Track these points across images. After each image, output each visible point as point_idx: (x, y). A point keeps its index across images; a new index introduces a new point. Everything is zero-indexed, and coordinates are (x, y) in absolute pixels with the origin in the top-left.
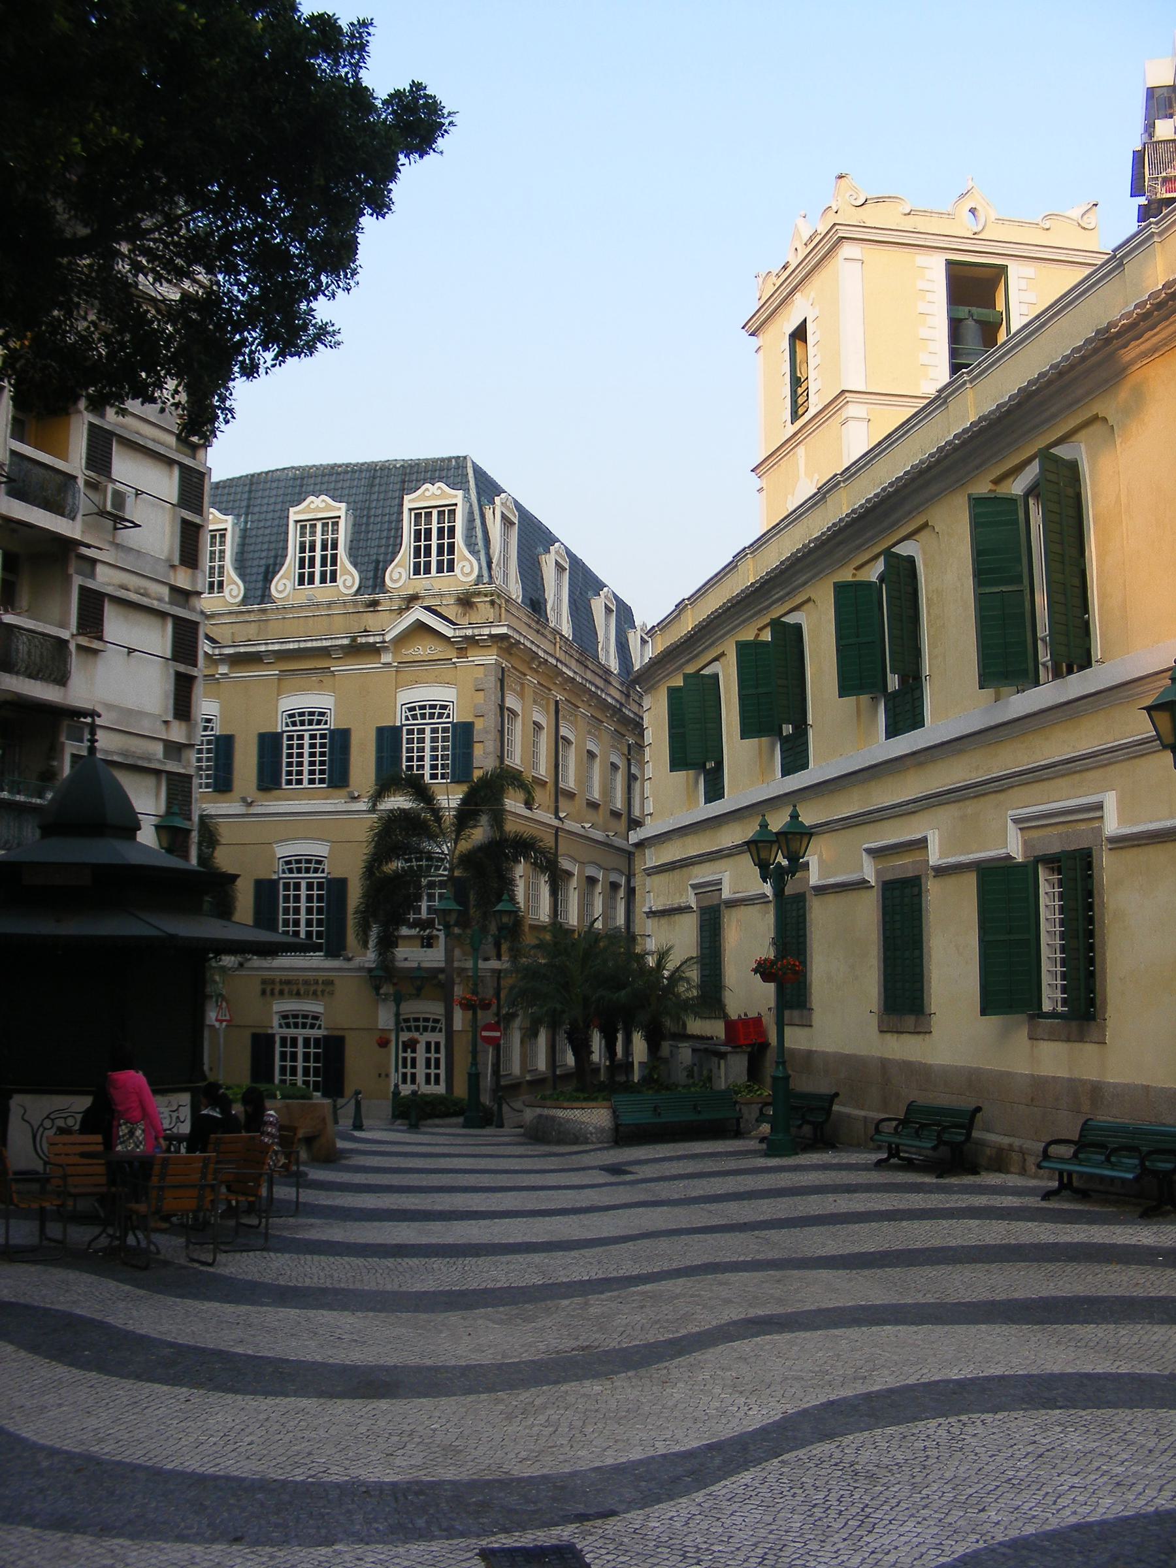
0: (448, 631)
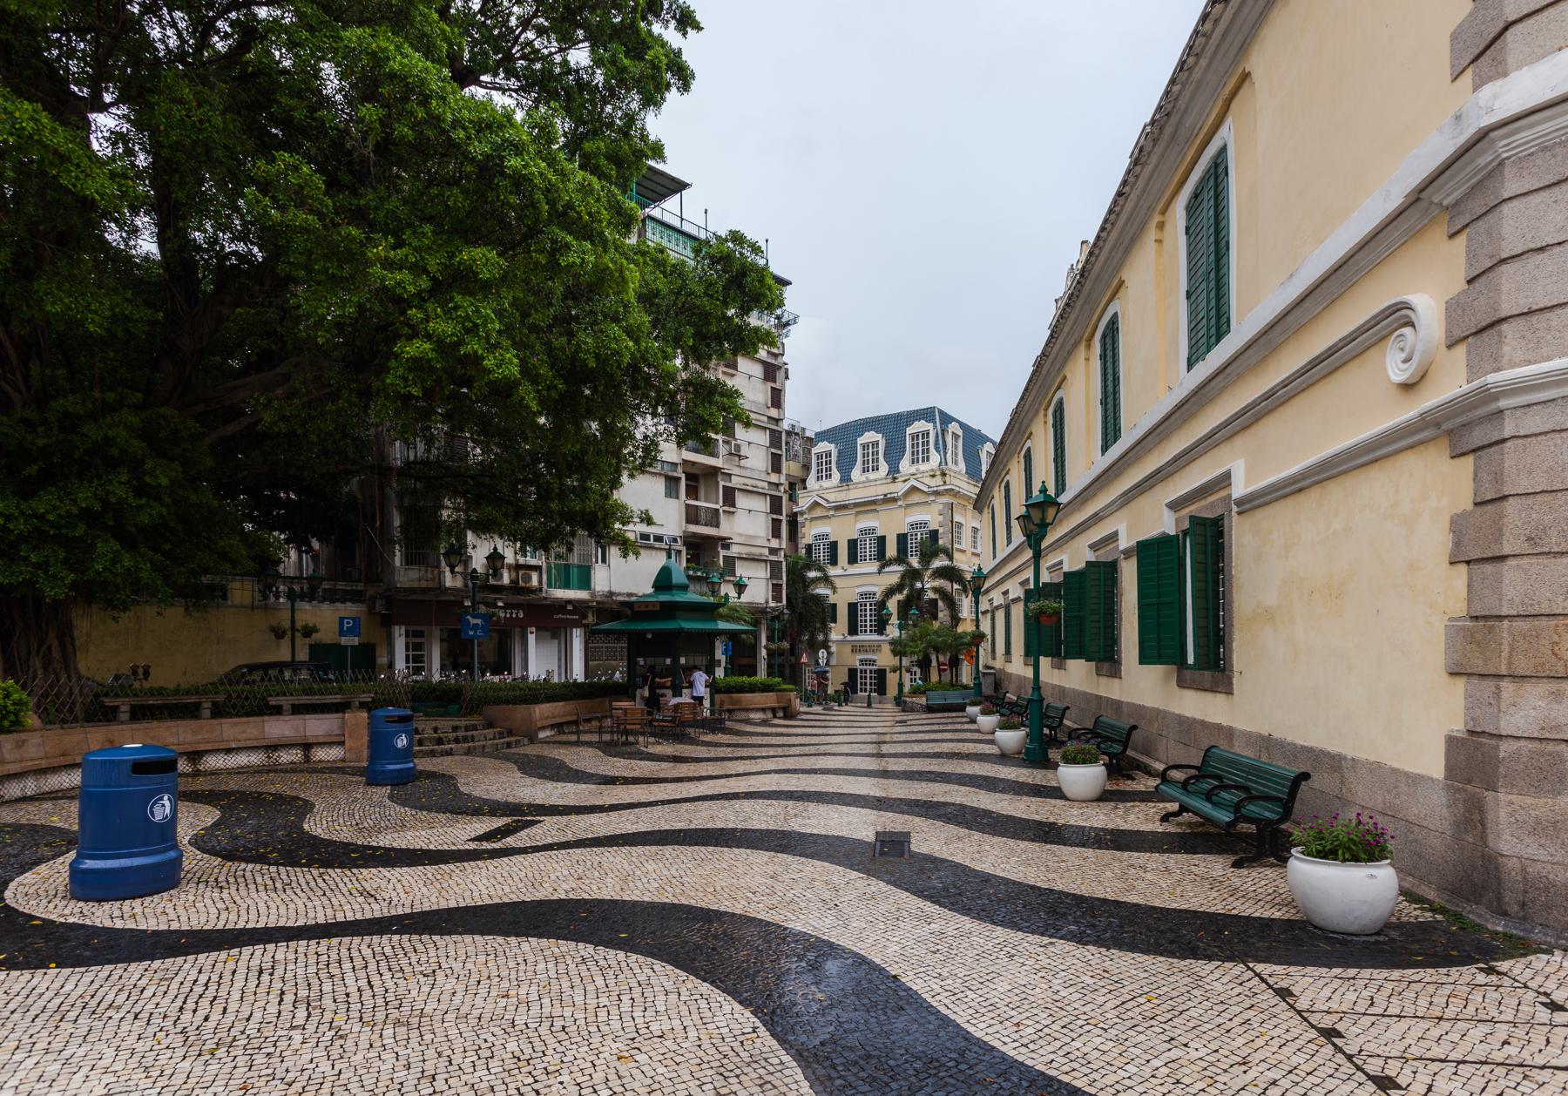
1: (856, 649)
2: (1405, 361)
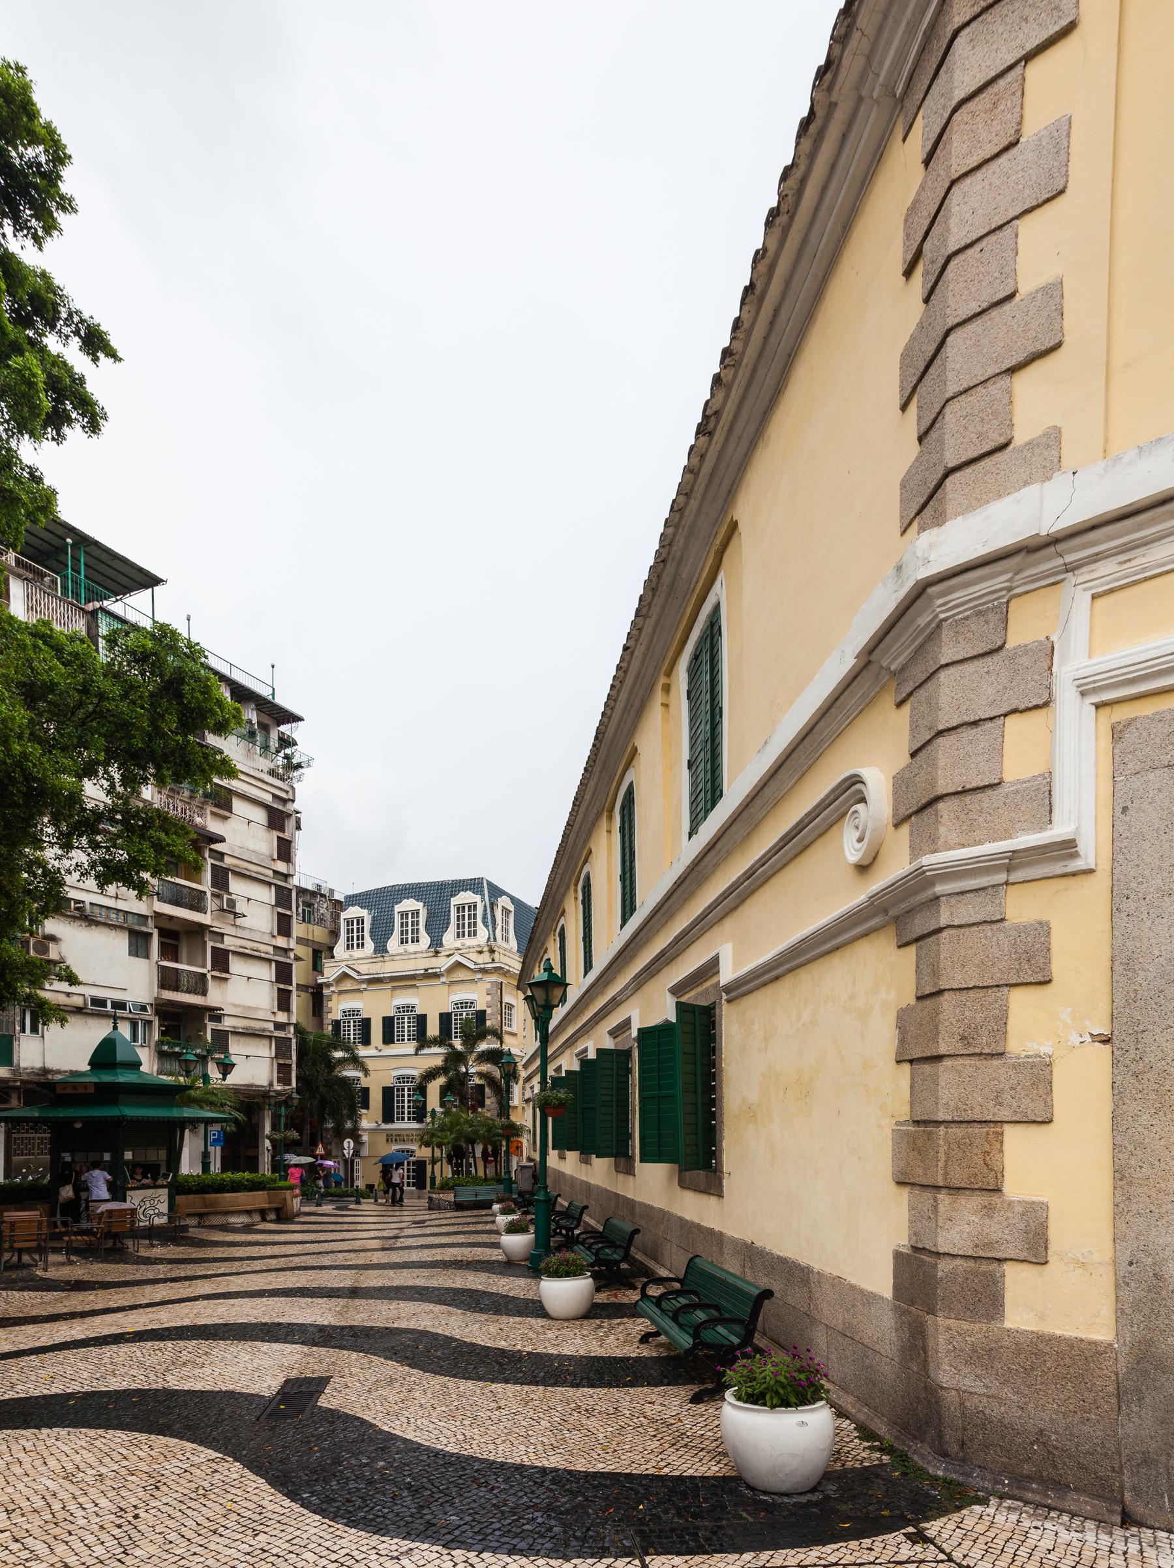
0: (472, 966)
1: (391, 1138)
2: (860, 840)
